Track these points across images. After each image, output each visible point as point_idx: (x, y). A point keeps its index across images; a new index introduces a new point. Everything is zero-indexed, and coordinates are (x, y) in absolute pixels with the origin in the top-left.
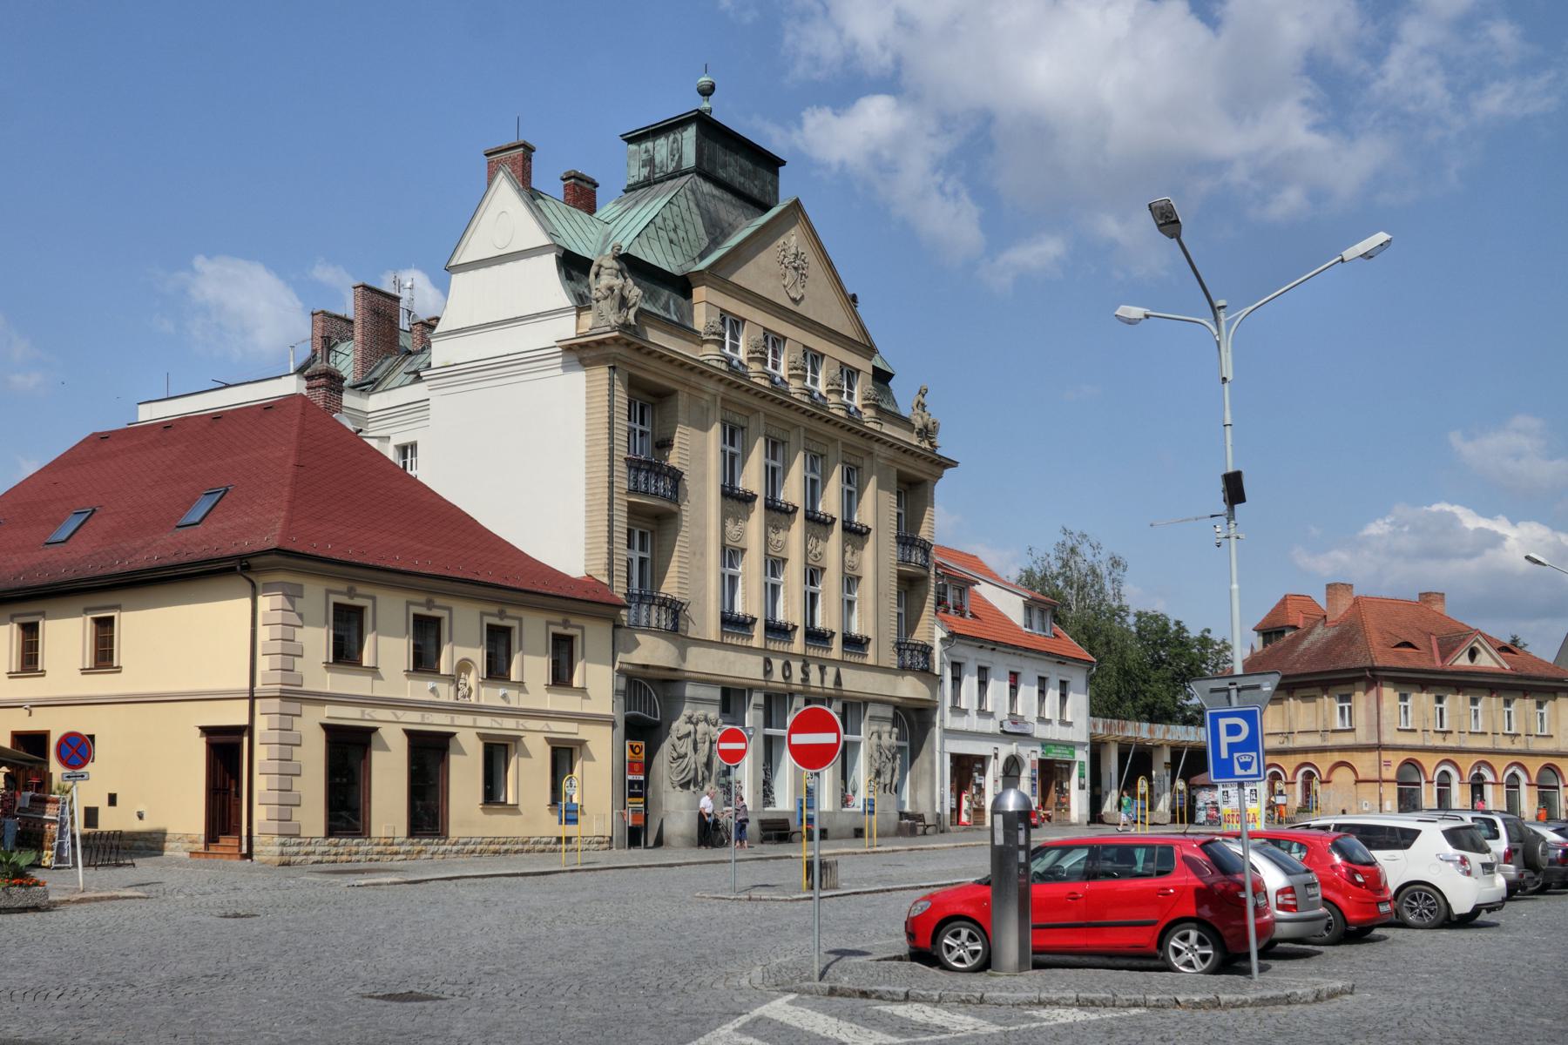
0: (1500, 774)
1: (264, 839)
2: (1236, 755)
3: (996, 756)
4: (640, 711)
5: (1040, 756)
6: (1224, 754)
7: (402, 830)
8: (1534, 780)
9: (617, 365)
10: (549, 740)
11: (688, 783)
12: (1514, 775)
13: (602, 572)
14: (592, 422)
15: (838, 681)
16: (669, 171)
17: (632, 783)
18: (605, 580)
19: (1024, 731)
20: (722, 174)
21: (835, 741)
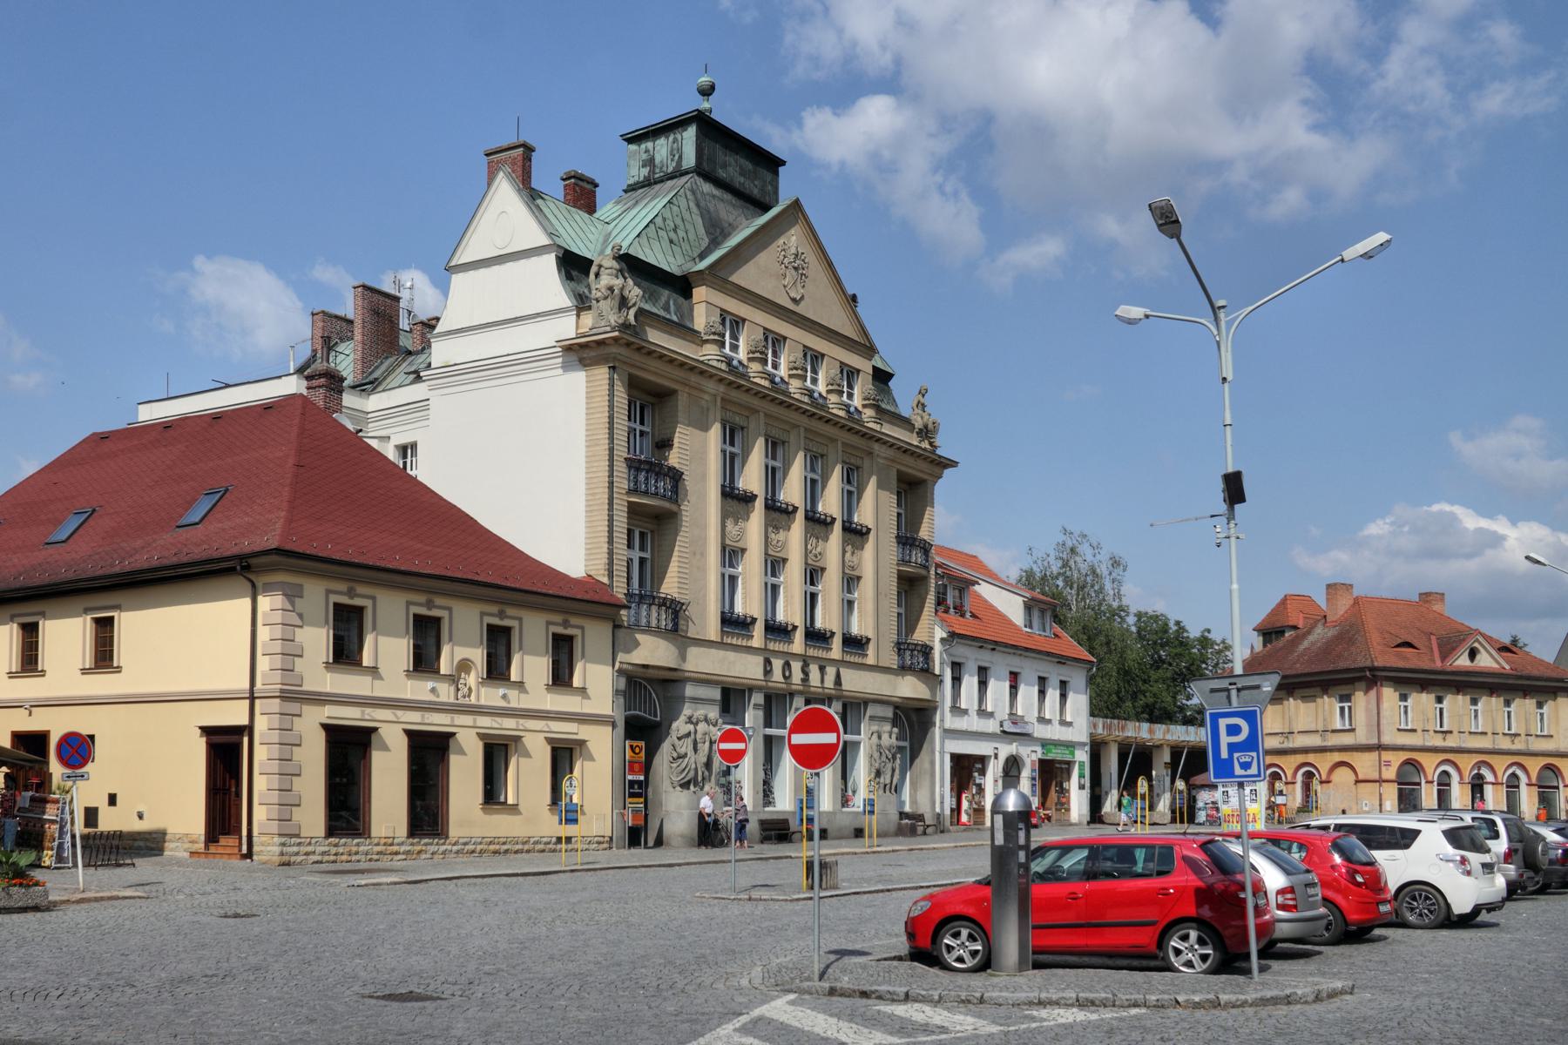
0: (1500, 774)
1: (264, 839)
2: (1236, 755)
3: (996, 756)
4: (640, 711)
5: (1040, 756)
6: (1224, 754)
7: (402, 830)
8: (1534, 780)
9: (617, 365)
10: (549, 740)
11: (688, 783)
12: (1514, 775)
13: (602, 572)
14: (592, 422)
15: (838, 681)
16: (669, 171)
17: (632, 783)
18: (605, 580)
19: (1024, 731)
20: (722, 174)
21: (835, 741)
